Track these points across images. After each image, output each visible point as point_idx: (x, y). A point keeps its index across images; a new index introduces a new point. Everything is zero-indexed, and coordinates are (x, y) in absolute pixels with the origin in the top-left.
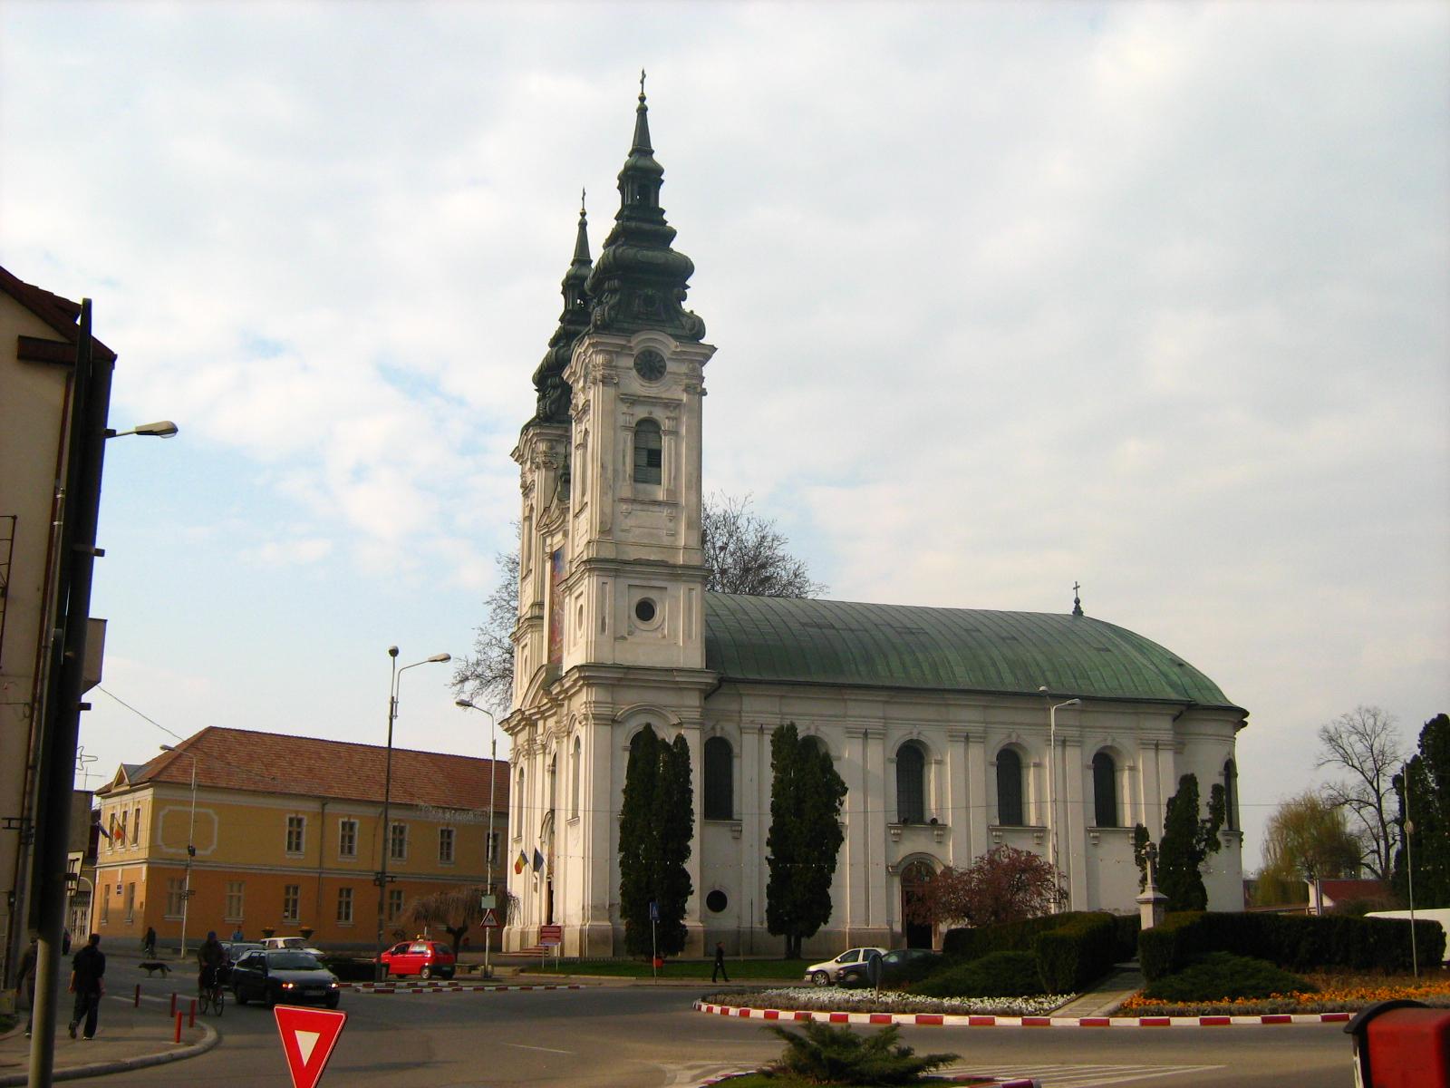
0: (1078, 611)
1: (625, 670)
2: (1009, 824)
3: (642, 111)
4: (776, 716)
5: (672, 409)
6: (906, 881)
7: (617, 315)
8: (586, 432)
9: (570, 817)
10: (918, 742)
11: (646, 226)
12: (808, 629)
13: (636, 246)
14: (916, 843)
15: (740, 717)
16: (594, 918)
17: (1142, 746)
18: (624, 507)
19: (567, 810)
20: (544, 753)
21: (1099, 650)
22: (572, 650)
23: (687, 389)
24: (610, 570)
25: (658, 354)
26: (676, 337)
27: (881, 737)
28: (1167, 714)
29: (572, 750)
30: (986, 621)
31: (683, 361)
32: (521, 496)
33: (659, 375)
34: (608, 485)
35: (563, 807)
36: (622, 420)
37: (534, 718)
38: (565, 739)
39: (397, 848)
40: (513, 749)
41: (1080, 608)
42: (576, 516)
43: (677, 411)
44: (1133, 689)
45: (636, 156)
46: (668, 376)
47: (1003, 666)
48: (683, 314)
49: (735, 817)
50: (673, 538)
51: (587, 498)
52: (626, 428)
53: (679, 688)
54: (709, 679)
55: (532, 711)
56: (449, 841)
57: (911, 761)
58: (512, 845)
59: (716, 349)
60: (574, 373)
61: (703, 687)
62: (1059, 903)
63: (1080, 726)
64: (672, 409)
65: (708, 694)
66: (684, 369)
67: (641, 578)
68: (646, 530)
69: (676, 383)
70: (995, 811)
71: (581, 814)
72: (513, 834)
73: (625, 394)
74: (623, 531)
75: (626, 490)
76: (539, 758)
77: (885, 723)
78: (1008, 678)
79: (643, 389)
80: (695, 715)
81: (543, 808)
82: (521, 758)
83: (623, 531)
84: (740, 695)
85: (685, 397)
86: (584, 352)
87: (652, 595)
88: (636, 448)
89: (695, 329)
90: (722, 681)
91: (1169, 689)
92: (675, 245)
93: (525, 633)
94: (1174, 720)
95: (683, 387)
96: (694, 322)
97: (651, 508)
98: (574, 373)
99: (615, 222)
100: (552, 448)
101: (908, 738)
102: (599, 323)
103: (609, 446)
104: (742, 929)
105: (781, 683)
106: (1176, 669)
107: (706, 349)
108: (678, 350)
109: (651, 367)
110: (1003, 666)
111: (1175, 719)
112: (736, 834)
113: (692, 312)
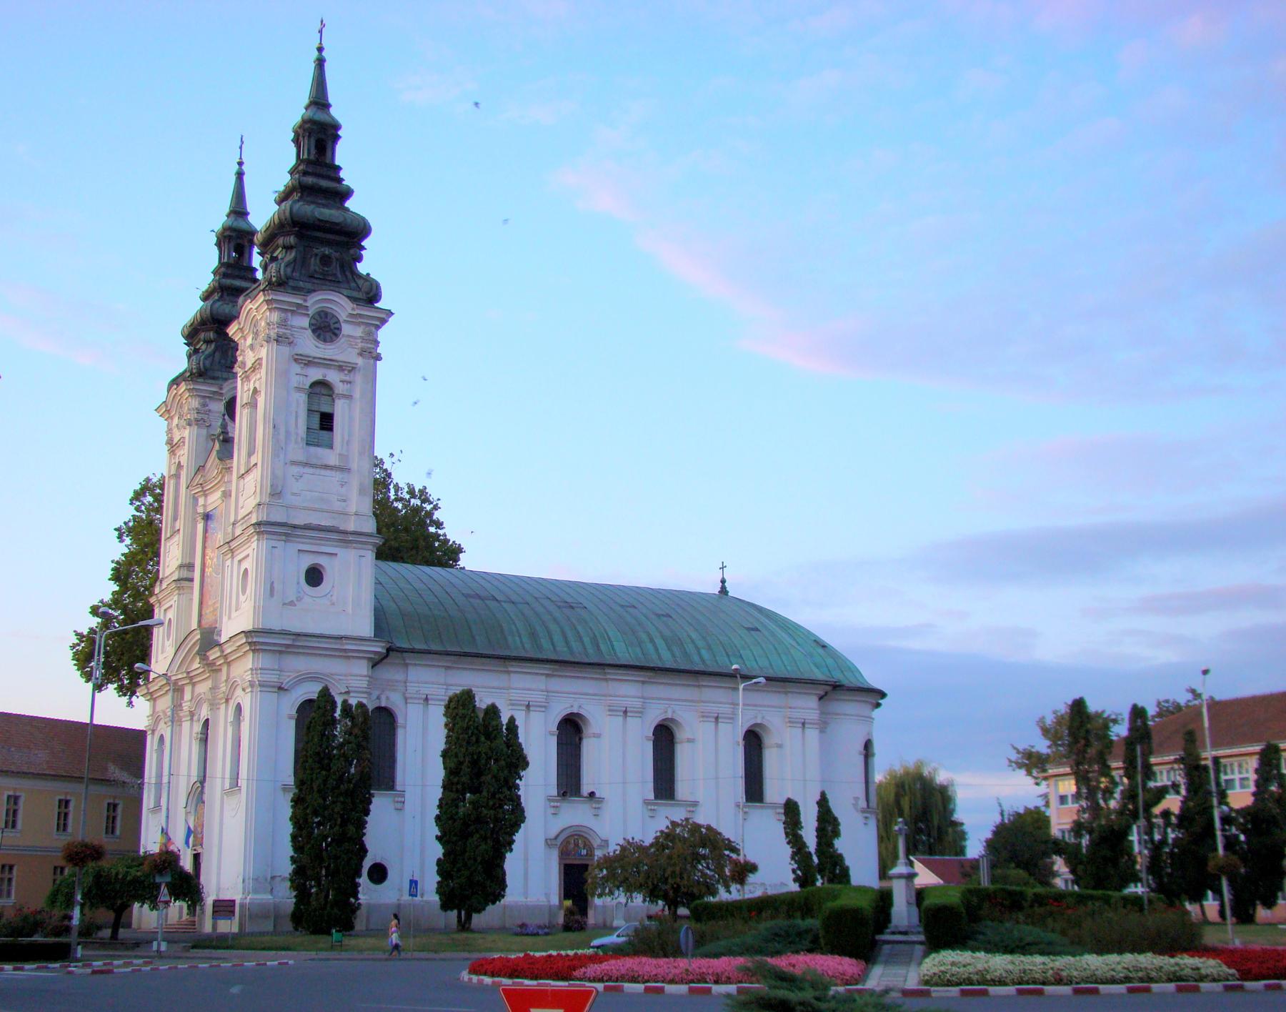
0: (724, 591)
1: (294, 637)
4: (441, 686)
5: (346, 372)
6: (564, 854)
7: (293, 272)
8: (255, 391)
9: (227, 786)
10: (578, 715)
11: (324, 183)
12: (471, 600)
13: (313, 203)
14: (574, 815)
15: (406, 687)
17: (789, 725)
18: (295, 470)
19: (223, 778)
20: (192, 719)
21: (749, 629)
22: (234, 614)
23: (362, 353)
24: (280, 534)
25: (334, 316)
27: (543, 709)
30: (568, 590)
31: (359, 324)
32: (167, 452)
33: (334, 337)
34: (278, 448)
35: (219, 775)
36: (295, 381)
37: (180, 684)
38: (223, 706)
39: (62, 822)
40: (152, 715)
41: (725, 588)
42: (242, 476)
43: (352, 374)
44: (783, 668)
45: (313, 109)
46: (343, 340)
47: (661, 643)
48: (360, 276)
49: (398, 787)
50: (344, 504)
52: (298, 389)
53: (346, 655)
54: (379, 648)
55: (180, 676)
56: (15, 807)
57: (571, 729)
58: (148, 816)
59: (392, 314)
61: (372, 656)
62: (62, 869)
63: (643, 698)
64: (346, 372)
65: (376, 662)
66: (358, 332)
67: (355, 644)
68: (317, 494)
69: (351, 346)
70: (651, 785)
71: (243, 783)
72: (148, 804)
73: (301, 355)
75: (297, 451)
76: (186, 725)
77: (447, 689)
78: (561, 646)
80: (363, 684)
81: (189, 776)
82: (162, 725)
84: (406, 665)
85: (360, 361)
87: (322, 561)
88: (309, 410)
89: (369, 294)
90: (389, 650)
91: (816, 670)
95: (357, 351)
96: (372, 285)
97: (323, 472)
99: (289, 177)
100: (204, 405)
101: (569, 711)
102: (274, 279)
104: (402, 902)
105: (448, 654)
106: (820, 650)
107: (381, 313)
108: (355, 313)
109: (325, 328)
110: (661, 643)
111: (821, 698)
112: (399, 805)
113: (368, 275)
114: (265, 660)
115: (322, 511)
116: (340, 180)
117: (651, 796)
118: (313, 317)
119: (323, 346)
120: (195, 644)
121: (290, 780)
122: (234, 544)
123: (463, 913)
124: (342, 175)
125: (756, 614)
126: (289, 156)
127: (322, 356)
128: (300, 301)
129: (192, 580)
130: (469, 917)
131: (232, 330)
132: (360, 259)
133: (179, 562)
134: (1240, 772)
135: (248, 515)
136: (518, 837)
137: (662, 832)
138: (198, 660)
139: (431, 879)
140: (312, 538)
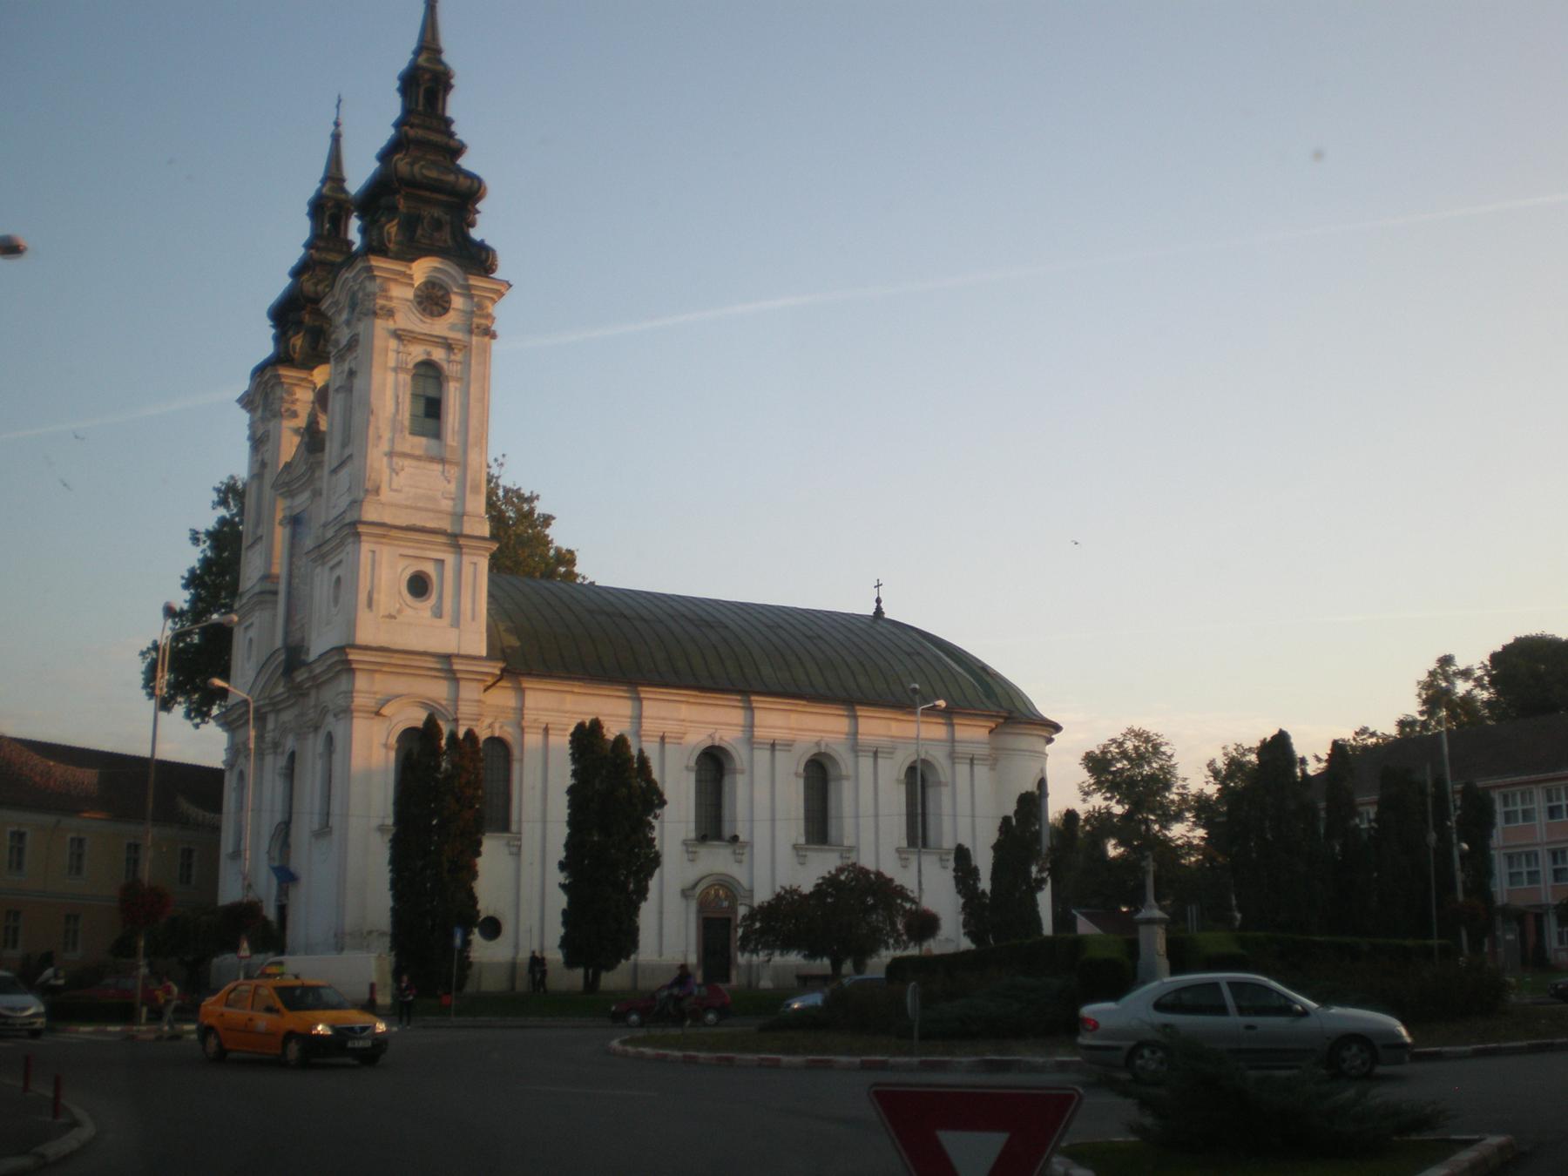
0: (879, 612)
2: (813, 843)
3: (336, 138)
6: (703, 906)
11: (434, 137)
14: (716, 860)
42: (334, 471)
49: (514, 827)
60: (336, 303)
67: (413, 548)
76: (269, 759)
79: (422, 325)
86: (354, 277)
89: (479, 260)
92: (465, 162)
94: (990, 732)
98: (336, 303)
115: (427, 510)
116: (451, 135)
117: (802, 840)
118: (418, 288)
119: (429, 321)
120: (277, 666)
121: (390, 821)
122: (326, 548)
123: (590, 971)
124: (454, 128)
125: (916, 636)
126: (393, 107)
127: (428, 332)
128: (402, 269)
129: (275, 593)
130: (596, 976)
131: (324, 305)
132: (472, 225)
133: (261, 573)
134: (1523, 802)
135: (340, 515)
136: (653, 884)
137: (823, 878)
138: (282, 684)
139: (556, 931)
140: (417, 541)
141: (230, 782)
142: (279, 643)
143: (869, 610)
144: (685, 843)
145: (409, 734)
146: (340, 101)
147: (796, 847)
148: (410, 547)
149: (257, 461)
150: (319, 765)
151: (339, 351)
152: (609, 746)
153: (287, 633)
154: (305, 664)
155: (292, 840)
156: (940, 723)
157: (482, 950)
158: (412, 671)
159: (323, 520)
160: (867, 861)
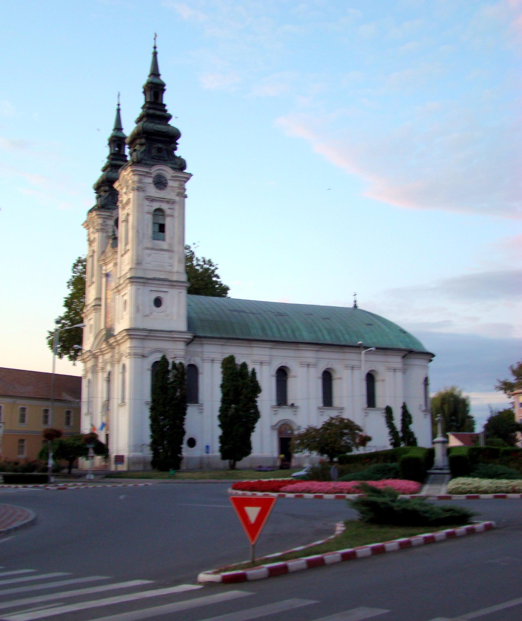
11: (159, 113)
14: (285, 414)
16: (135, 451)
26: (174, 169)
28: (399, 355)
29: (121, 371)
36: (147, 209)
47: (325, 332)
51: (129, 247)
52: (148, 213)
53: (174, 340)
54: (189, 336)
61: (185, 340)
65: (189, 343)
66: (176, 184)
69: (173, 191)
71: (127, 401)
74: (147, 263)
75: (148, 242)
83: (147, 263)
85: (177, 199)
87: (161, 295)
90: (195, 337)
93: (91, 313)
95: (176, 194)
100: (104, 222)
103: (139, 221)
106: (402, 334)
111: (404, 357)
112: (200, 411)
114: (136, 343)
116: (166, 111)
122: (120, 288)
124: (166, 108)
128: (147, 170)
129: (100, 305)
132: (176, 149)
140: (156, 284)
141: (84, 383)
142: (102, 326)
143: (351, 305)
144: (273, 407)
145: (156, 364)
146: (119, 95)
147: (319, 408)
148: (155, 287)
149: (90, 250)
150: (120, 376)
151: (123, 205)
152: (239, 367)
153: (106, 323)
154: (113, 336)
155: (110, 408)
156: (314, 350)
157: (186, 452)
158: (136, 337)
159: (118, 276)
160: (346, 415)
